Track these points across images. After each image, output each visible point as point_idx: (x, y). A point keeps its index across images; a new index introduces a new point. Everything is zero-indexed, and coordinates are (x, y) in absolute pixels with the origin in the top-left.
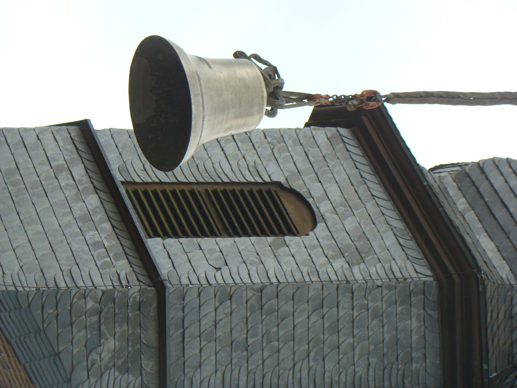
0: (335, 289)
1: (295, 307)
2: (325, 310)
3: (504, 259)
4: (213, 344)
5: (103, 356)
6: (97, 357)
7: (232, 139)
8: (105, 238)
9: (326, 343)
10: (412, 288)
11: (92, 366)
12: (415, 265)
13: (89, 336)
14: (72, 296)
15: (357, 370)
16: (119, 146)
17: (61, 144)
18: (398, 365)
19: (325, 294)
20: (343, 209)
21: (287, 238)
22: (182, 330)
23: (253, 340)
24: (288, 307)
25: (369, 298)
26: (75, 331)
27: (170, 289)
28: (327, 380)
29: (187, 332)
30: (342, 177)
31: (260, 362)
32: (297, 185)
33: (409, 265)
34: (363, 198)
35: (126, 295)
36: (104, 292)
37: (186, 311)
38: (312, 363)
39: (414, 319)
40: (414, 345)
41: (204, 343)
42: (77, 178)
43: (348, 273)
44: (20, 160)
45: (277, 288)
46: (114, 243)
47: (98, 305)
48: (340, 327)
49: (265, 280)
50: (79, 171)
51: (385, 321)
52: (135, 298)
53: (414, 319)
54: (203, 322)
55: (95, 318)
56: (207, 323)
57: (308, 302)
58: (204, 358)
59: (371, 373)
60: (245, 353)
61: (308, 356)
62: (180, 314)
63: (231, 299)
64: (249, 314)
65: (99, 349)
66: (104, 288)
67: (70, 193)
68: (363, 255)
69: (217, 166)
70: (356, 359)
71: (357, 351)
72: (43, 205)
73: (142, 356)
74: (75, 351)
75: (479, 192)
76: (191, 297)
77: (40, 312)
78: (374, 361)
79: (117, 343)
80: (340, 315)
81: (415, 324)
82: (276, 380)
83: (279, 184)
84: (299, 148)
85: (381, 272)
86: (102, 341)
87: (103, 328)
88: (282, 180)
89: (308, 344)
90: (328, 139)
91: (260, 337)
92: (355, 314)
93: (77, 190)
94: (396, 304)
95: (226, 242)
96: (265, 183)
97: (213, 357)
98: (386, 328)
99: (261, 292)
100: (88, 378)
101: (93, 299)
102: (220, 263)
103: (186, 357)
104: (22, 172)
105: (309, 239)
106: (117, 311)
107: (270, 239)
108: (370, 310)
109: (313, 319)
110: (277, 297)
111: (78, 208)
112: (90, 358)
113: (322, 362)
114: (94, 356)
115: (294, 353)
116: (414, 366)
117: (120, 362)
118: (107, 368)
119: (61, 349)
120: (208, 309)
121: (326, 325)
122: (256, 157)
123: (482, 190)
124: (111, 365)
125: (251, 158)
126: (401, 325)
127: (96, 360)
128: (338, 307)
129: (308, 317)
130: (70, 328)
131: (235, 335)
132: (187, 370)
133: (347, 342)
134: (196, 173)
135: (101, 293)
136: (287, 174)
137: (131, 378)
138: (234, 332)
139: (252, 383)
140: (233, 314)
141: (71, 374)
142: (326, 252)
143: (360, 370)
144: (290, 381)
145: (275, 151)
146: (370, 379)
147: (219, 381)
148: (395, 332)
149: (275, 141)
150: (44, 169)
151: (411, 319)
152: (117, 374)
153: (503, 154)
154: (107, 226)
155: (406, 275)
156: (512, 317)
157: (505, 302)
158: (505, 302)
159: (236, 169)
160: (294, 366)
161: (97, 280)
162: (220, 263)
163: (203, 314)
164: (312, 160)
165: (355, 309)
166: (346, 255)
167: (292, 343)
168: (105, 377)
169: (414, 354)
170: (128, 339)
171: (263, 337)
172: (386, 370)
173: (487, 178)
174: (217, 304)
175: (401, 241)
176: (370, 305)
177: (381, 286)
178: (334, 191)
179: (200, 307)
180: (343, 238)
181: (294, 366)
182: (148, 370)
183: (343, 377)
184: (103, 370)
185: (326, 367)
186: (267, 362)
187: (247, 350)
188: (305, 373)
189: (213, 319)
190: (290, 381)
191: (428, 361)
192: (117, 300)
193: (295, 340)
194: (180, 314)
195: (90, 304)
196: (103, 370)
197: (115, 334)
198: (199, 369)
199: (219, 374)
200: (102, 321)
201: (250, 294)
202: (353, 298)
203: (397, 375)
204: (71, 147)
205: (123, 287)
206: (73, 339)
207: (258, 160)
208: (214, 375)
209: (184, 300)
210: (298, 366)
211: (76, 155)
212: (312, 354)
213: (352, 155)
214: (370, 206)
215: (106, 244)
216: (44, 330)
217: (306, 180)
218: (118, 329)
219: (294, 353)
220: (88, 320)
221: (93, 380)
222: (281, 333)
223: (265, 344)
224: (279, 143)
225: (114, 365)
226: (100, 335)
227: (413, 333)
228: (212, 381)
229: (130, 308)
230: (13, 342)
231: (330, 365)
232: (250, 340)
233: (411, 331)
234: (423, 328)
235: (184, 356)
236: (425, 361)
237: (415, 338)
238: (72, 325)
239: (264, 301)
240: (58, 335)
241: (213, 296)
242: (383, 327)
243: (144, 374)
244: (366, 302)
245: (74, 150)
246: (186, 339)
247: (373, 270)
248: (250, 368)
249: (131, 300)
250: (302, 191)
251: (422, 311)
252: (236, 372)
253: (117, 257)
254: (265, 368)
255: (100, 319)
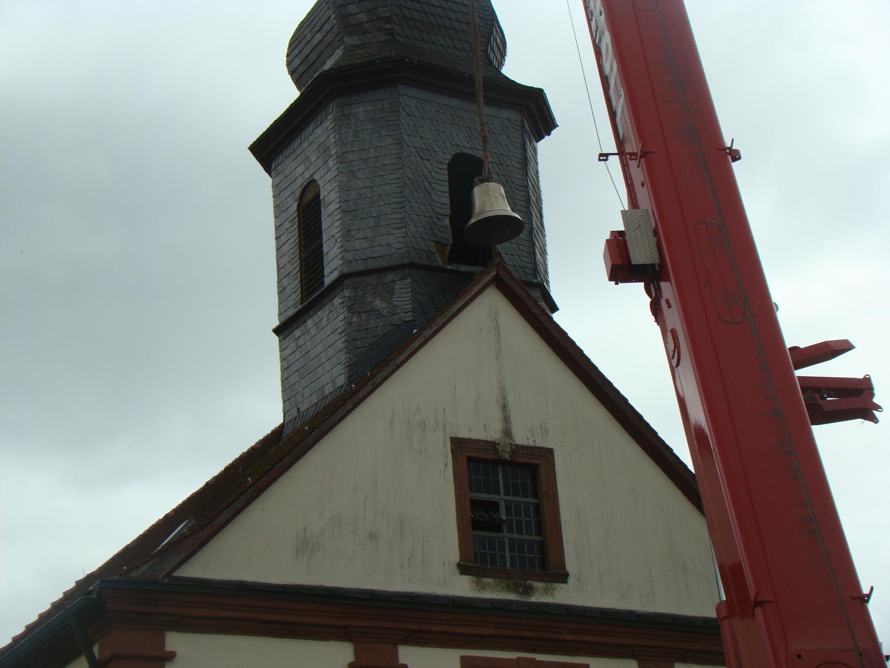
0: (342, 165)
1: (354, 189)
2: (354, 169)
3: (334, 53)
4: (377, 239)
5: (384, 307)
6: (385, 310)
7: (279, 239)
8: (325, 313)
9: (374, 165)
10: (339, 115)
11: (390, 313)
12: (329, 113)
13: (373, 317)
14: (350, 331)
15: (390, 143)
16: (285, 309)
17: (286, 346)
18: (386, 117)
19: (345, 170)
20: (307, 164)
21: (321, 198)
22: (369, 260)
23: (373, 212)
24: (354, 194)
25: (346, 141)
26: (370, 327)
27: (346, 270)
28: (396, 162)
29: (370, 256)
30: (294, 165)
31: (386, 206)
32: (298, 194)
33: (329, 118)
34: (302, 150)
35: (349, 298)
36: (348, 312)
37: (358, 258)
38: (386, 173)
39: (358, 111)
40: (374, 108)
41: (376, 244)
42: (300, 334)
43: (335, 156)
44: (295, 369)
45: (343, 202)
46: (327, 308)
47: (355, 315)
48: (365, 158)
49: (338, 211)
50: (297, 333)
51: (360, 129)
52: (350, 292)
53: (358, 111)
54: (364, 246)
55: (363, 315)
56: (365, 244)
57: (350, 181)
58: (385, 243)
59: (390, 133)
60: (381, 217)
61: (382, 176)
62: (359, 262)
63: (350, 231)
64: (359, 218)
65: (381, 309)
66: (346, 313)
67: (307, 337)
68: (326, 148)
69: (292, 246)
70: (383, 144)
71: (378, 144)
72: (313, 353)
73: (385, 282)
74: (382, 324)
75: (304, 73)
76: (349, 256)
77: (359, 349)
78: (384, 133)
79: (377, 299)
80: (357, 159)
81: (361, 109)
82: (398, 194)
83: (298, 206)
84: (282, 194)
85: (333, 135)
86: (376, 309)
87: (368, 310)
88: (296, 203)
89: (375, 177)
90: (277, 176)
91: (372, 209)
92: (357, 149)
93: (306, 334)
94: (349, 124)
95: (325, 237)
96: (298, 215)
97: (384, 237)
98: (363, 128)
99: (345, 212)
100: (397, 314)
101: (351, 317)
102: (333, 239)
103: (384, 254)
104: (299, 368)
105: (321, 183)
106: (358, 302)
107: (322, 209)
108: (354, 140)
109: (360, 176)
110: (348, 201)
111: (313, 332)
112: (385, 315)
113: (386, 166)
114: (385, 312)
115: (381, 185)
116: (386, 106)
117: (388, 296)
118: (391, 303)
119: (380, 334)
120: (357, 244)
121: (364, 167)
122: (287, 222)
123: (302, 72)
124: (390, 301)
125: (287, 225)
126: (362, 118)
127: (387, 311)
128: (353, 161)
129: (359, 179)
130: (369, 330)
131: (371, 225)
132: (392, 253)
133: (373, 152)
134: (295, 259)
135: (348, 314)
136: (294, 201)
137: (397, 287)
138: (370, 226)
139: (399, 210)
140: (359, 228)
141: (395, 325)
142: (326, 172)
143: (390, 141)
144: (397, 185)
145: (284, 209)
146: (394, 134)
147: (398, 231)
148: (367, 122)
149: (279, 211)
150: (298, 355)
151: (358, 112)
152: (395, 296)
153: (284, 60)
154: (320, 313)
155: (333, 120)
156: (363, 44)
157: (353, 51)
158: (353, 51)
159: (293, 234)
160: (388, 184)
161: (342, 317)
162: (333, 239)
163: (359, 248)
164: (286, 186)
165: (354, 150)
166: (327, 159)
167: (375, 188)
168: (396, 303)
169: (379, 107)
170: (374, 293)
171: (372, 207)
172: (389, 124)
173: (296, 68)
174: (353, 239)
175: (319, 124)
176: (351, 140)
177: (340, 135)
178: (300, 170)
179: (355, 250)
180: (320, 162)
181: (388, 184)
182: (392, 277)
183: (394, 151)
184: (393, 305)
185: (389, 163)
186: (387, 202)
187: (380, 216)
188: (392, 177)
189: (362, 240)
190: (397, 185)
191: (382, 98)
192: (352, 303)
193: (373, 185)
194: (359, 262)
195: (355, 319)
196: (393, 305)
197: (372, 301)
198: (392, 245)
199: (394, 232)
200: (364, 310)
201: (347, 219)
202: (347, 152)
203: (392, 116)
204: (287, 339)
205: (344, 301)
206: (374, 327)
207: (288, 220)
208: (395, 235)
209: (351, 261)
210: (388, 182)
211: (291, 336)
212: (381, 173)
213: (283, 160)
214: (305, 145)
215: (328, 313)
216: (370, 345)
217: (295, 189)
218: (369, 300)
219: (381, 185)
220: (364, 319)
221: (398, 311)
222: (369, 195)
223: (376, 205)
224: (280, 208)
225: (390, 299)
226: (373, 310)
227: (366, 110)
228: (398, 235)
229: (357, 294)
230: (375, 364)
231: (388, 161)
232: (374, 215)
233: (365, 111)
234: (364, 104)
235: (384, 256)
236: (383, 99)
237: (369, 108)
238: (367, 329)
239: (350, 209)
240: (372, 336)
241: (348, 243)
242: (364, 130)
243: (394, 280)
244: (349, 143)
245: (289, 337)
246: (374, 256)
247: (333, 141)
248: (390, 212)
249: (351, 294)
250: (300, 190)
251: (353, 106)
252: (392, 221)
253: (333, 305)
254: (390, 202)
255: (364, 312)
